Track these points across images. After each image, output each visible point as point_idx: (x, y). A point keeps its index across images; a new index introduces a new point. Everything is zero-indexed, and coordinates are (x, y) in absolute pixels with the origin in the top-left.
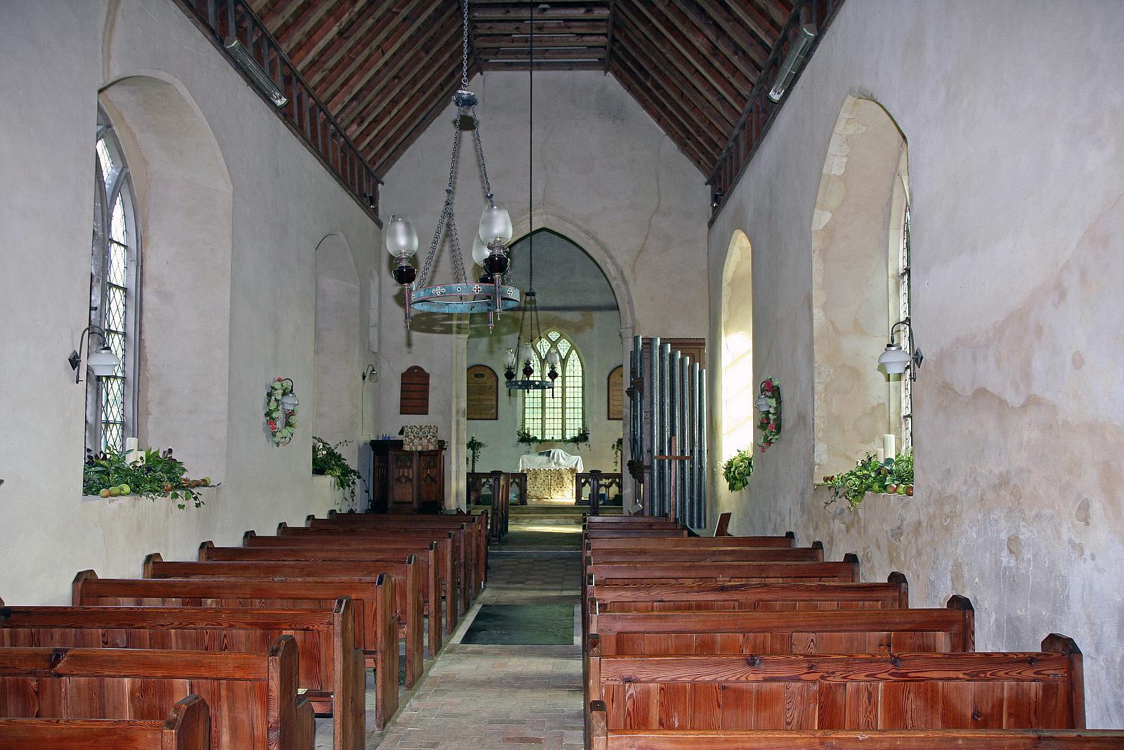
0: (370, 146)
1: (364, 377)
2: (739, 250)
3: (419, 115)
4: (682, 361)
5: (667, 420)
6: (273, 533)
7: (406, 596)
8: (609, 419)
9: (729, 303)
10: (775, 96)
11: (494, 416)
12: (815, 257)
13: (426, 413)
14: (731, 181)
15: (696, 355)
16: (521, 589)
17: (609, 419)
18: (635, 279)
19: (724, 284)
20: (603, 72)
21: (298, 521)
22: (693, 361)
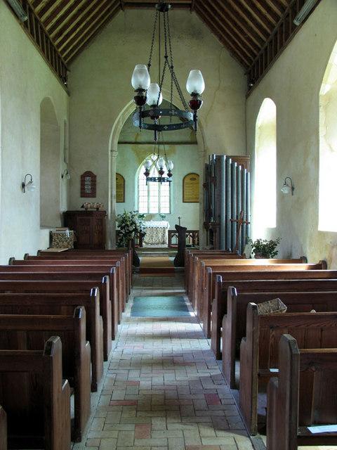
0: (64, 50)
1: (62, 177)
2: (267, 112)
3: (271, 15)
4: (238, 168)
5: (235, 200)
6: (22, 258)
7: (142, 273)
8: (184, 202)
9: (259, 138)
10: (297, 23)
11: (122, 200)
12: (321, 109)
13: (95, 197)
14: (262, 73)
15: (245, 165)
16: (152, 289)
17: (184, 202)
18: (207, 126)
19: (256, 128)
20: (189, 12)
21: (34, 253)
22: (243, 168)
